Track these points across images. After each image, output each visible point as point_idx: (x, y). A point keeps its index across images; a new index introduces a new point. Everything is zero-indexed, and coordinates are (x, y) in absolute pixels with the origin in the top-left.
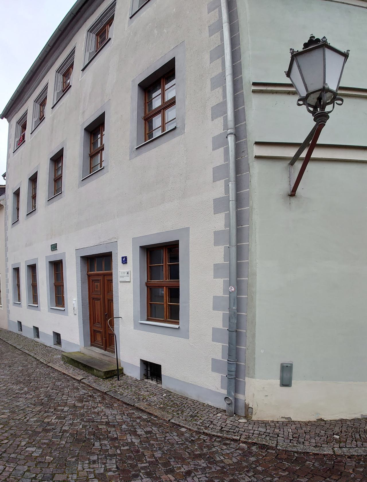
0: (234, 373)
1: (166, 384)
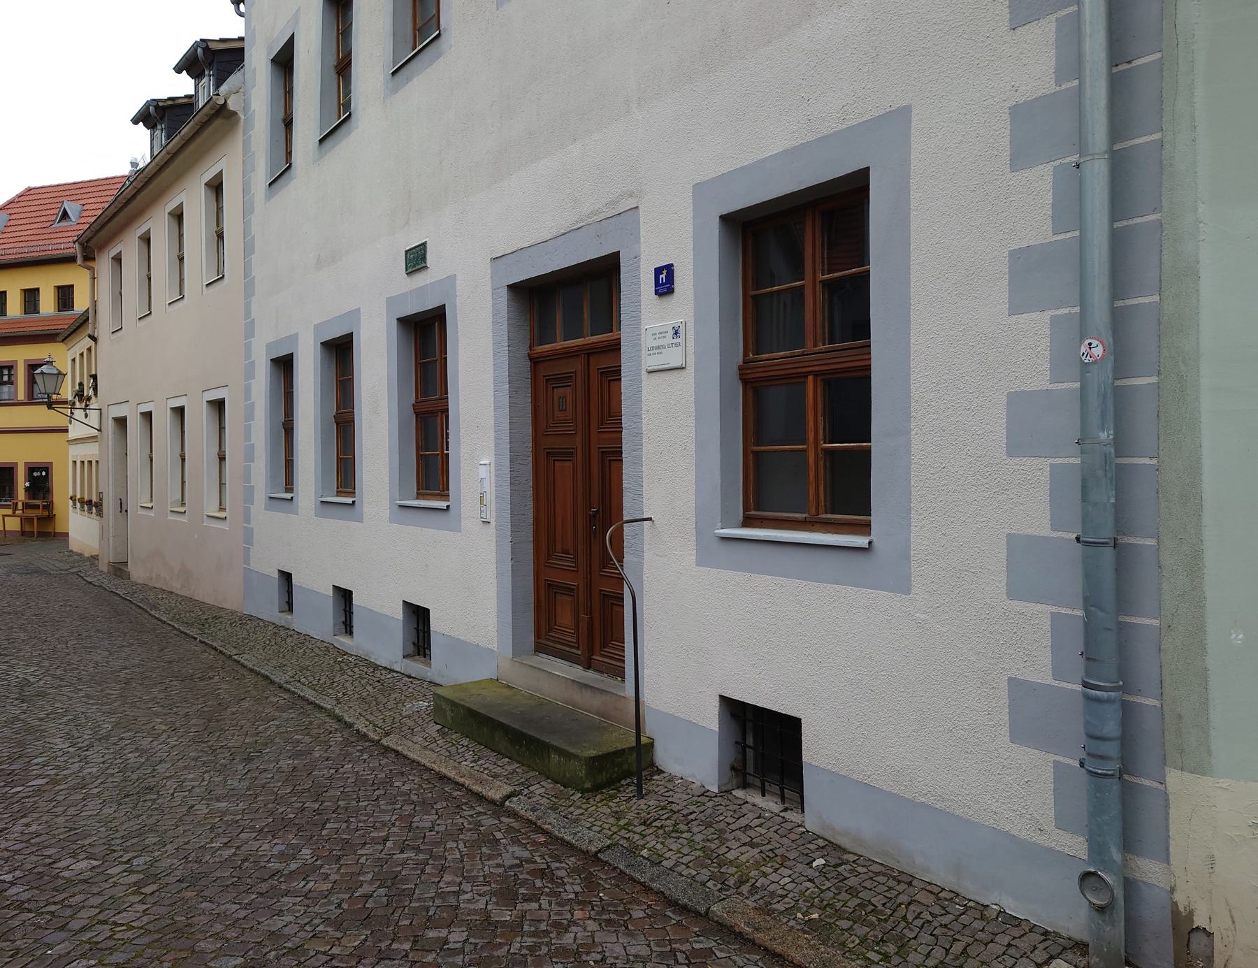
0: (1112, 749)
1: (823, 810)
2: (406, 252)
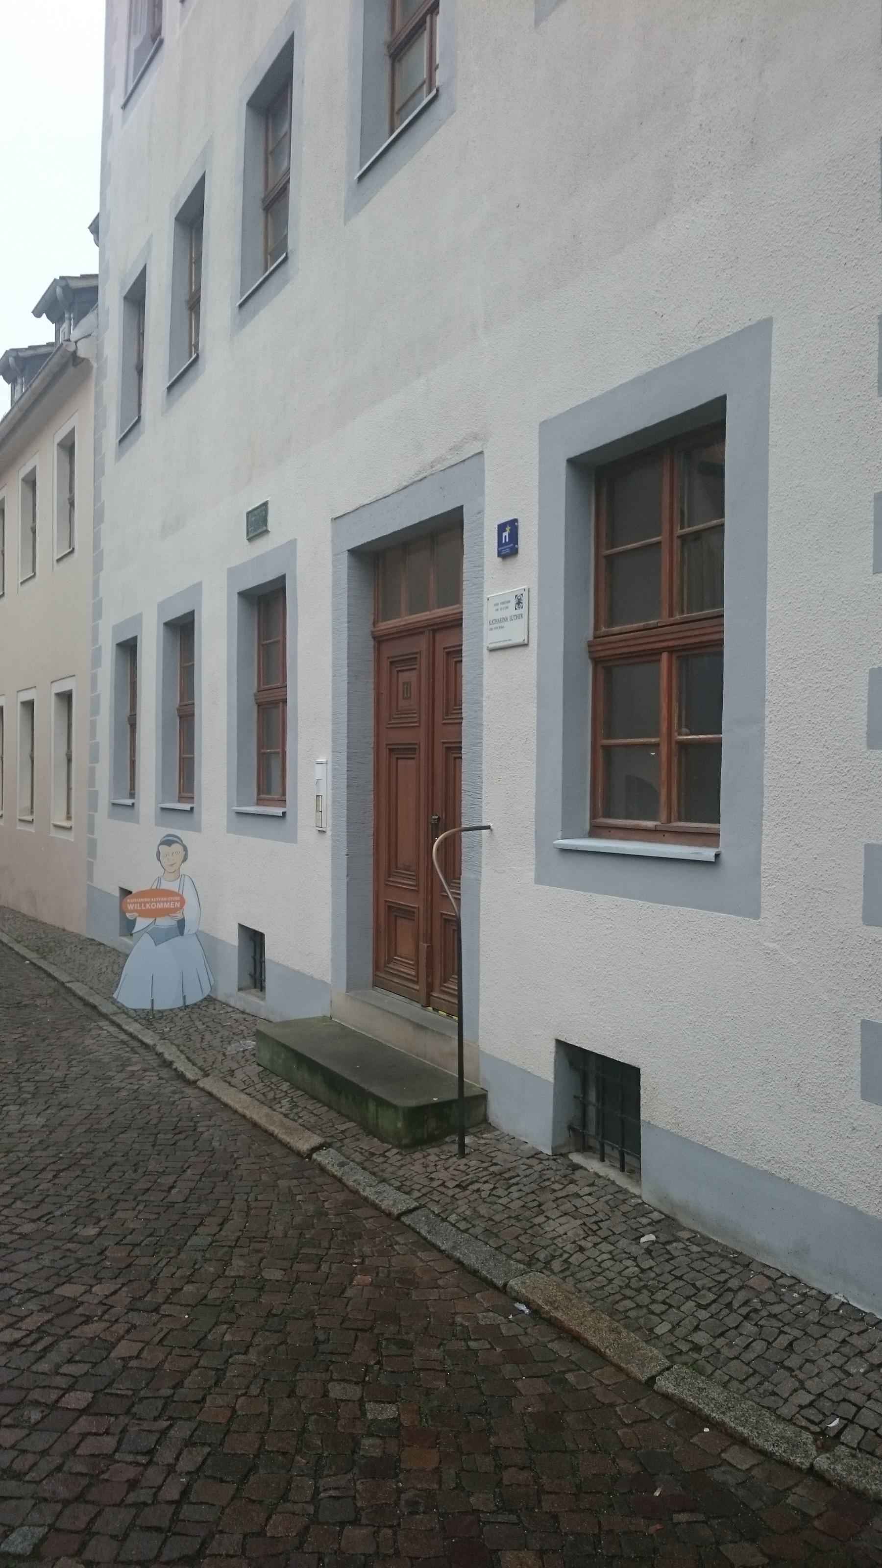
2: (248, 514)
